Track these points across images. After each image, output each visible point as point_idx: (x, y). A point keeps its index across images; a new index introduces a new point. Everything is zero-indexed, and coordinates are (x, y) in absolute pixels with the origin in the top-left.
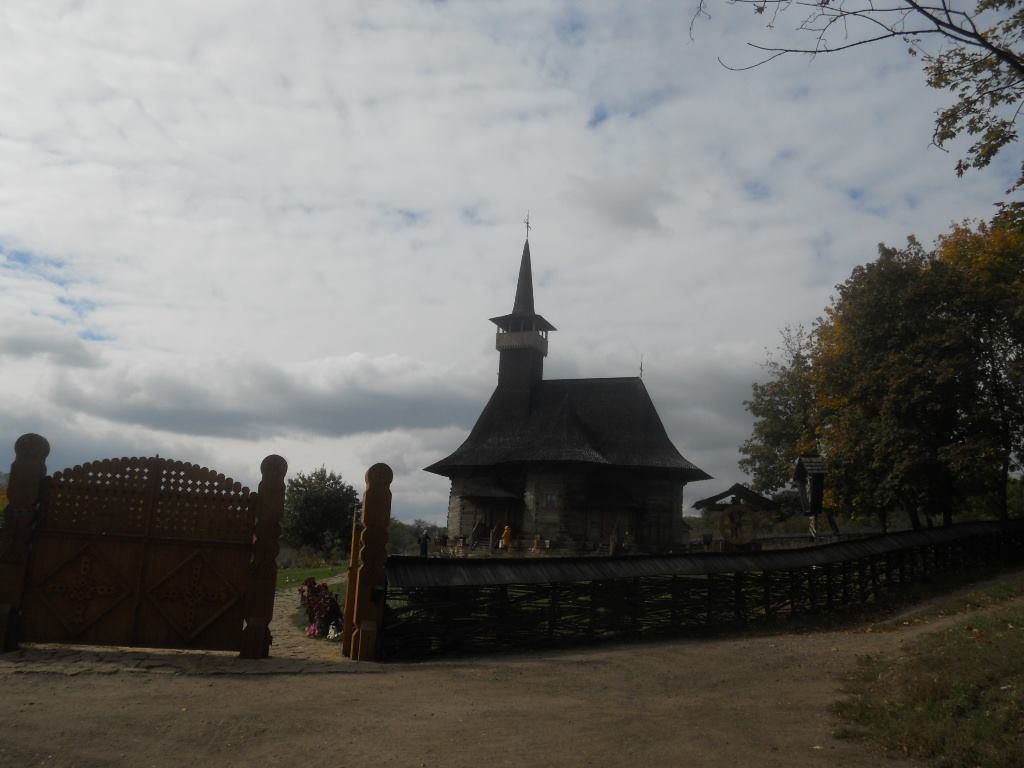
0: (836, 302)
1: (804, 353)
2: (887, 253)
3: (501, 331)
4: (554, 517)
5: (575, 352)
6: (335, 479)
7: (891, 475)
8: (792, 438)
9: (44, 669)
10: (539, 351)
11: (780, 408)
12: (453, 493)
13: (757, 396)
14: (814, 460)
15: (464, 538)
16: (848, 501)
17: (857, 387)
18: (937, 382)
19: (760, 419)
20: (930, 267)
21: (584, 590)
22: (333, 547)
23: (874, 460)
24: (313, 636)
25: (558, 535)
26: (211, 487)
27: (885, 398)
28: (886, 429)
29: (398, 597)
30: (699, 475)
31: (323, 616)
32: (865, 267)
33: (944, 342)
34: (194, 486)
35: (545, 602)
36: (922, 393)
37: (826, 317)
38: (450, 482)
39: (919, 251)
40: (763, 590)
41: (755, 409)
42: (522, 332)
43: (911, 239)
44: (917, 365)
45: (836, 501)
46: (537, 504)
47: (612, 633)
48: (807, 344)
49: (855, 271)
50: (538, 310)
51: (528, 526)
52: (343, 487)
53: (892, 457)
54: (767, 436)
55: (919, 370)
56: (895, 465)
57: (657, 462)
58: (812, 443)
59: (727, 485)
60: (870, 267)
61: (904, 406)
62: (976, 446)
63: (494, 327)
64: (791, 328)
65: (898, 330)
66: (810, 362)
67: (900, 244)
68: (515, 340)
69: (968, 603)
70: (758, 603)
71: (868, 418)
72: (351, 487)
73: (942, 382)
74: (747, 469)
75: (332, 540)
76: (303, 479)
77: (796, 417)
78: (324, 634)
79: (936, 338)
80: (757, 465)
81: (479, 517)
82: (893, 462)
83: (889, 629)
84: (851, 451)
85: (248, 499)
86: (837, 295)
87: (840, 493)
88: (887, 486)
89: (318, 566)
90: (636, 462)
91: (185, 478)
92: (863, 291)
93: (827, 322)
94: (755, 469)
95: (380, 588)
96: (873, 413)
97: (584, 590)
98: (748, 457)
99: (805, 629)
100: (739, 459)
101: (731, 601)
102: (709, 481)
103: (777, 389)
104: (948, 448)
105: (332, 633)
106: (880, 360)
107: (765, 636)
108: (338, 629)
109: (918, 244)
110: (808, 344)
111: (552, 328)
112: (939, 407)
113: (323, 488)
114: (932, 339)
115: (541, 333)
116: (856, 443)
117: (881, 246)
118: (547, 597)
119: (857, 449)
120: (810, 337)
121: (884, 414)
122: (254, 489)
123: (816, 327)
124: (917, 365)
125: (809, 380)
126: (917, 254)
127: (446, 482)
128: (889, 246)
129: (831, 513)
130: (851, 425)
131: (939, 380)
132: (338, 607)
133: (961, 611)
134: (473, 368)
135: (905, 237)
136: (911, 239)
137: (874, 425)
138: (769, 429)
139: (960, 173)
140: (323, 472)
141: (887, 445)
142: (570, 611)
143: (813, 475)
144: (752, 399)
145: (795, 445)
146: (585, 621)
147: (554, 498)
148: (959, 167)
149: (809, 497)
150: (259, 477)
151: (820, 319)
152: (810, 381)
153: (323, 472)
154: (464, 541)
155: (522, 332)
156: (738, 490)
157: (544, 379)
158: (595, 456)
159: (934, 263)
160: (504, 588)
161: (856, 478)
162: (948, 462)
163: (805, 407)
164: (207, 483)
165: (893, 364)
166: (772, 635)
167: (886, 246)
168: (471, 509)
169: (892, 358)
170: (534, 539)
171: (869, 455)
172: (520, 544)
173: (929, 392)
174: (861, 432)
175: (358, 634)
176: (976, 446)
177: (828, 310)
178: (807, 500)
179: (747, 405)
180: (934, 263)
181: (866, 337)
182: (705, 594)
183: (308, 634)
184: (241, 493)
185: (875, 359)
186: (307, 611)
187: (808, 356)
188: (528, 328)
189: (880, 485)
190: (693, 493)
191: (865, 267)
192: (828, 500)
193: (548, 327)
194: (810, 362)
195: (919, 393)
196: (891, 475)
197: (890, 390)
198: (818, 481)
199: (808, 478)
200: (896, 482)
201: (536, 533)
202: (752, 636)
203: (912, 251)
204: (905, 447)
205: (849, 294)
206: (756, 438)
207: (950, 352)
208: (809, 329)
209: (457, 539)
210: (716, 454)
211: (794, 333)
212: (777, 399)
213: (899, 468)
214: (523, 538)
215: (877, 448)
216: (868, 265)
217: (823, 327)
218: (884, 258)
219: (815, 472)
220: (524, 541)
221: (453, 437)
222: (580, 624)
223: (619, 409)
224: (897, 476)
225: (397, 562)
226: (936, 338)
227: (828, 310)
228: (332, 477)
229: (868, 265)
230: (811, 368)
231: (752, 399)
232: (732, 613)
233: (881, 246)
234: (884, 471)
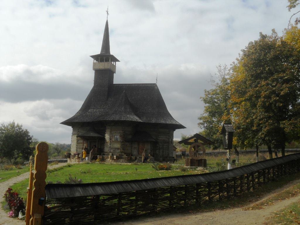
0: (241, 56)
1: (227, 77)
2: (263, 37)
3: (95, 61)
4: (118, 145)
5: (126, 72)
6: (19, 127)
7: (260, 133)
8: (220, 114)
11: (216, 100)
12: (73, 134)
13: (206, 95)
14: (229, 125)
15: (78, 154)
16: (243, 143)
17: (248, 94)
18: (281, 94)
19: (207, 105)
20: (280, 43)
21: (133, 194)
22: (18, 157)
23: (254, 126)
24: (11, 216)
25: (120, 153)
27: (259, 100)
28: (259, 113)
29: (52, 202)
30: (181, 127)
31: (16, 208)
32: (254, 42)
33: (285, 76)
35: (116, 201)
36: (275, 98)
37: (236, 62)
38: (72, 129)
39: (276, 36)
40: (208, 190)
41: (205, 101)
42: (105, 59)
43: (273, 31)
44: (273, 86)
45: (238, 142)
46: (111, 139)
47: (144, 212)
48: (228, 73)
49: (249, 44)
50: (112, 53)
51: (106, 149)
52: (23, 131)
53: (261, 125)
54: (210, 112)
55: (274, 89)
56: (263, 129)
57: (163, 121)
58: (228, 116)
59: (193, 134)
60: (256, 42)
61: (267, 104)
62: (296, 121)
64: (221, 65)
65: (266, 71)
66: (229, 81)
67: (268, 33)
69: (291, 193)
70: (205, 195)
71: (252, 107)
72: (27, 130)
73: (283, 94)
74: (201, 127)
75: (18, 154)
76: (4, 127)
77: (222, 105)
78: (17, 216)
79: (281, 75)
80: (206, 125)
81: (85, 145)
82: (262, 127)
83: (259, 207)
84: (244, 122)
86: (242, 53)
87: (240, 139)
88: (259, 137)
89: (12, 169)
90: (153, 121)
92: (253, 53)
93: (237, 64)
94: (204, 127)
95: (43, 199)
96: (254, 106)
97: (133, 194)
98: (201, 121)
99: (225, 207)
100: (198, 123)
101: (194, 195)
102: (185, 129)
103: (214, 92)
104: (284, 122)
105: (20, 216)
106: (259, 83)
108: (23, 214)
109: (276, 33)
110: (229, 74)
111: (118, 61)
112: (282, 104)
113: (13, 131)
114: (280, 75)
115: (113, 63)
116: (247, 118)
117: (261, 33)
118: (117, 199)
119: (247, 121)
120: (229, 70)
121: (259, 107)
123: (231, 66)
124: (273, 86)
125: (228, 89)
126: (275, 37)
127: (70, 129)
128: (264, 34)
129: (235, 147)
130: (245, 111)
131: (282, 93)
132: (23, 204)
133: (287, 198)
134: (84, 76)
136: (273, 31)
137: (254, 111)
138: (210, 110)
140: (14, 123)
141: (260, 120)
142: (127, 204)
143: (229, 132)
144: (204, 96)
145: (221, 117)
146: (133, 208)
147: (118, 137)
148: (296, 21)
149: (227, 141)
151: (234, 63)
152: (229, 90)
153: (14, 123)
154: (78, 156)
155: (105, 59)
156: (197, 136)
157: (114, 83)
158: (136, 119)
159: (282, 42)
160: (98, 196)
161: (247, 133)
162: (284, 128)
163: (226, 100)
165: (264, 85)
166: (211, 211)
167: (263, 34)
168: (81, 141)
169: (263, 83)
170: (109, 155)
171: (252, 123)
172: (103, 157)
173: (278, 98)
174: (249, 114)
175: (33, 220)
176: (296, 121)
177: (237, 59)
178: (226, 143)
179: (202, 99)
180: (282, 42)
181: (253, 73)
182: (184, 193)
183: (9, 215)
185: (256, 83)
186: (9, 204)
187: (228, 79)
188: (107, 60)
189: (257, 137)
190: (177, 136)
191: (254, 42)
192: (235, 141)
193: (116, 60)
194: (229, 81)
195: (274, 98)
196: (260, 133)
197: (262, 96)
198: (231, 135)
199: (227, 133)
200: (263, 136)
201: (110, 152)
202: (203, 212)
203: (273, 36)
204: (267, 121)
205: (247, 54)
206: (205, 113)
207: (287, 81)
208: (229, 67)
209: (75, 155)
210: (188, 118)
211: (222, 68)
212: (214, 96)
213: (265, 130)
214: (104, 155)
215: (256, 121)
216: (255, 41)
217: (235, 66)
218: (262, 38)
219: (230, 131)
221: (75, 106)
222: (130, 209)
223: (145, 98)
224: (263, 134)
225: (51, 186)
226: (281, 75)
227: (237, 59)
228: (18, 126)
229: (255, 41)
230: (229, 84)
231: (204, 96)
232: (195, 200)
233: (261, 33)
234: (257, 131)
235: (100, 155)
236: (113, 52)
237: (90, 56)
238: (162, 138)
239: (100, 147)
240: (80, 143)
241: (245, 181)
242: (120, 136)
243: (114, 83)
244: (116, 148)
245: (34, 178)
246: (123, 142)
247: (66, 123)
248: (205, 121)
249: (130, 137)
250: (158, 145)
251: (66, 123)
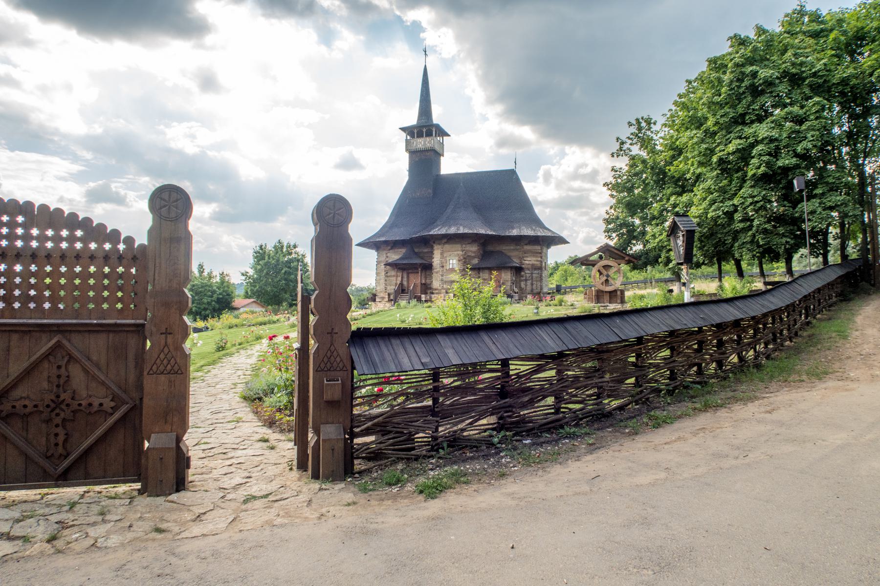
9: (376, 421)
10: (435, 155)
26: (72, 239)
30: (561, 241)
34: (42, 238)
50: (436, 119)
63: (404, 135)
68: (421, 143)
85: (135, 256)
91: (26, 226)
107: (64, 486)
122: (142, 239)
135: (792, 5)
139: (687, 81)
147: (455, 261)
150: (147, 220)
164: (65, 233)
168: (393, 273)
182: (696, 347)
184: (121, 247)
188: (429, 134)
214: (433, 293)
220: (433, 296)
235: (426, 293)
236: (437, 116)
238: (530, 261)
239: (423, 282)
240: (390, 276)
241: (169, 367)
245: (314, 310)
248: (612, 224)
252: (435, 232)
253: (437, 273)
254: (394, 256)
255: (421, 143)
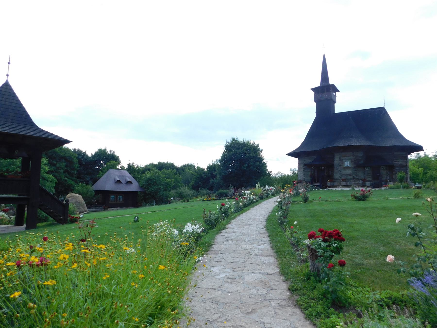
42: (325, 93)
68: (323, 96)
111: (338, 91)
147: (349, 163)
155: (325, 93)
157: (335, 112)
237: (71, 142)
242: (351, 162)
243: (335, 112)
244: (348, 174)
246: (355, 167)
247: (292, 154)
249: (362, 162)
250: (394, 170)
251: (292, 154)
252: (336, 145)
253: (337, 169)
254: (308, 160)
255: (323, 96)
